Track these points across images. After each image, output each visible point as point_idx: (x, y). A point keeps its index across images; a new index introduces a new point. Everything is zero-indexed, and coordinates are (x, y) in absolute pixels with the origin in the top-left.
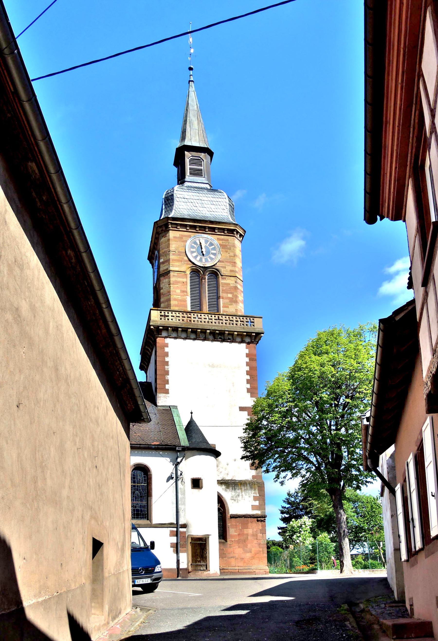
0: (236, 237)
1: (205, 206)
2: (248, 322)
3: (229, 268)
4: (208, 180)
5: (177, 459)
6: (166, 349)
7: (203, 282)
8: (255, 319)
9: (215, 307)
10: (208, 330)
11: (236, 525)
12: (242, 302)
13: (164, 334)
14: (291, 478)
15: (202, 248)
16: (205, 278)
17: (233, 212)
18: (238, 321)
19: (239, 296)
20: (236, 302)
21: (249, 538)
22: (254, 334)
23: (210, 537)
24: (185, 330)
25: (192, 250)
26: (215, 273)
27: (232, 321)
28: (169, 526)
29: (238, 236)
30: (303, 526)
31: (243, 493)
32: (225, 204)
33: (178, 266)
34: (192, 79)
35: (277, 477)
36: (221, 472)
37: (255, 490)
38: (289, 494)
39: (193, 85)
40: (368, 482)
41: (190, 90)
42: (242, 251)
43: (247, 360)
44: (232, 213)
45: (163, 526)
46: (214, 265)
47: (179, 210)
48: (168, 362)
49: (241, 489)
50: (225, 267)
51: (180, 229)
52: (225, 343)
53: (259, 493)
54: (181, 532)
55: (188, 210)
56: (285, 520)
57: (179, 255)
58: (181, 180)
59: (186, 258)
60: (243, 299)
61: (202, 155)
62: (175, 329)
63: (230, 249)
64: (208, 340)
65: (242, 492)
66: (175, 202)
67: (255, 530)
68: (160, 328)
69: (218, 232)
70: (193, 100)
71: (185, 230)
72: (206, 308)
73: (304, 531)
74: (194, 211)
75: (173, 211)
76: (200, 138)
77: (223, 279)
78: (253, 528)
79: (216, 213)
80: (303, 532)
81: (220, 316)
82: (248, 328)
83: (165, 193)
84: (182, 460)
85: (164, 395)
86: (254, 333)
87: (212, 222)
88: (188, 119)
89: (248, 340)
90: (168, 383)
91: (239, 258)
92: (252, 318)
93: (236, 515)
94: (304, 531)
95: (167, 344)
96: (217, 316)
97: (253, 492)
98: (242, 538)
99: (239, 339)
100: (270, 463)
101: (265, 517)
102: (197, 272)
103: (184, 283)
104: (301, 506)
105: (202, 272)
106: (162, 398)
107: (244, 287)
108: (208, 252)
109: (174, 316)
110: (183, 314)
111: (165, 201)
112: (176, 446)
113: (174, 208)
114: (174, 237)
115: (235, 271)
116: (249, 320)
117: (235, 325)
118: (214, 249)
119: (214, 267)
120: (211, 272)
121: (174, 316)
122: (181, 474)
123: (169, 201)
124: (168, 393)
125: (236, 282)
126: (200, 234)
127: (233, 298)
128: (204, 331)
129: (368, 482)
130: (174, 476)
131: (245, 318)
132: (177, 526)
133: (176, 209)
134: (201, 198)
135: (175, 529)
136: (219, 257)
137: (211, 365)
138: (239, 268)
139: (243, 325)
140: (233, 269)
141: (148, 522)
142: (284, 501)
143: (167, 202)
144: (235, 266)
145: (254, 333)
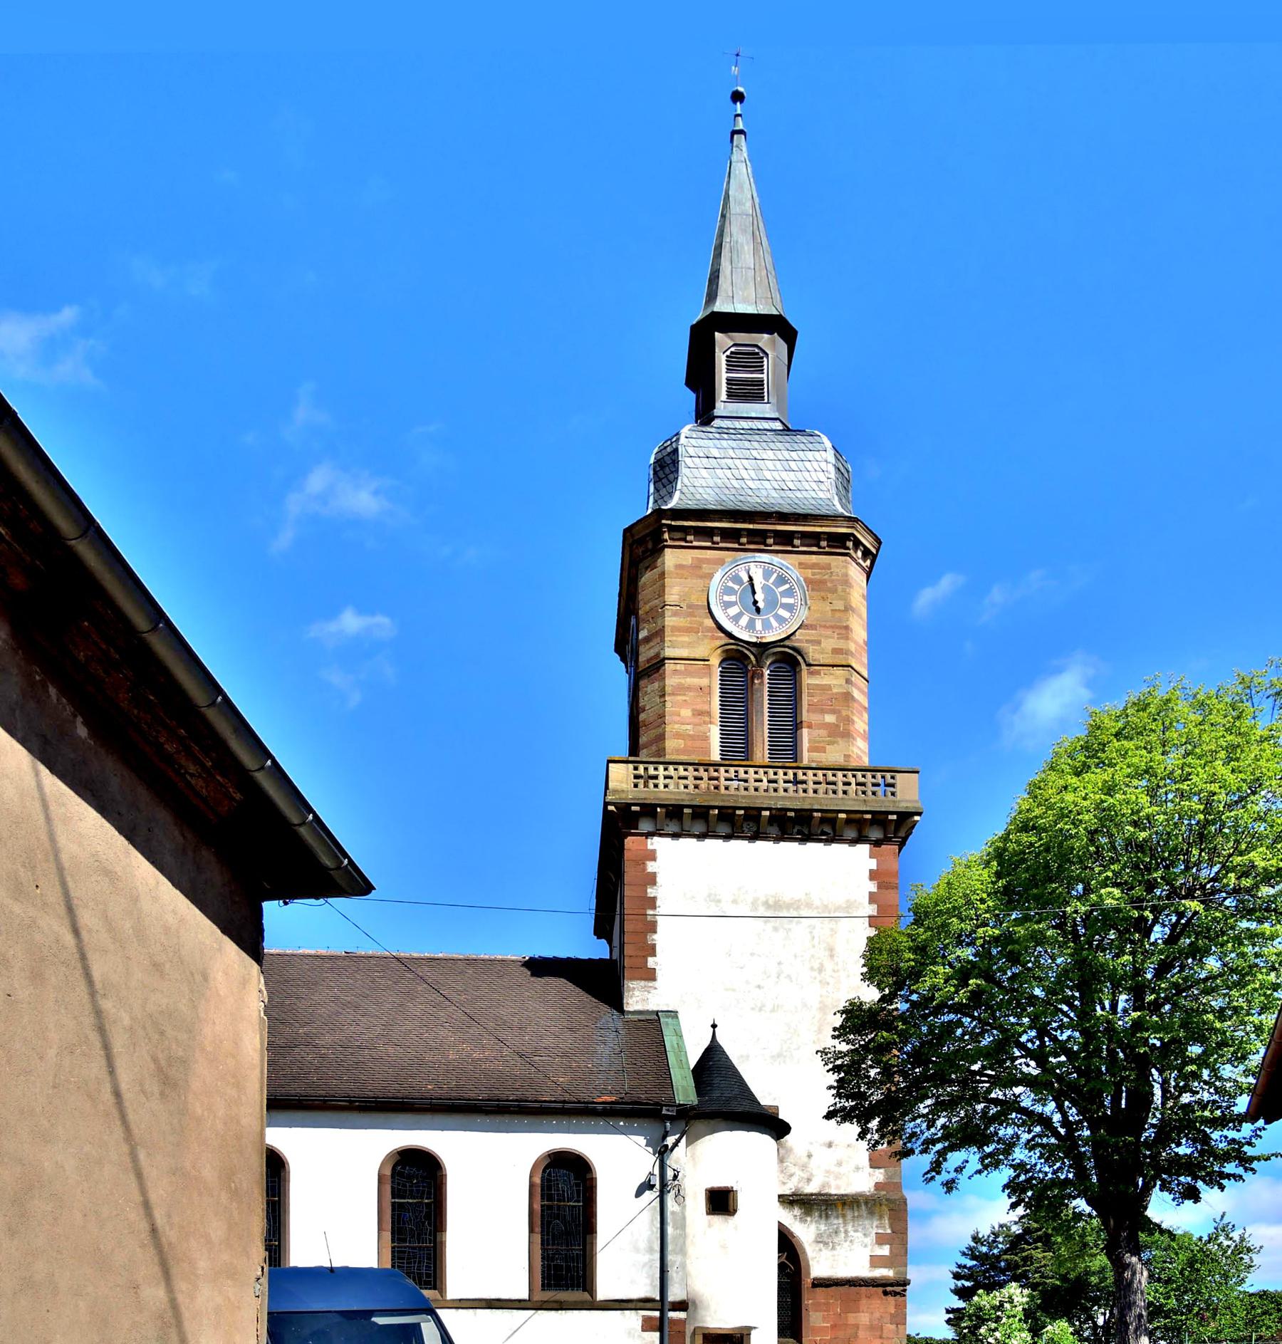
0: (852, 557)
1: (768, 475)
2: (878, 785)
3: (830, 643)
4: (778, 411)
5: (664, 1138)
6: (651, 867)
7: (756, 687)
8: (898, 775)
9: (786, 747)
10: (766, 809)
11: (828, 1304)
12: (863, 738)
13: (645, 826)
14: (979, 1172)
15: (754, 592)
16: (762, 675)
17: (847, 490)
18: (849, 784)
19: (856, 719)
20: (847, 735)
21: (861, 1334)
22: (895, 817)
23: (753, 1332)
24: (701, 813)
25: (726, 598)
26: (788, 660)
27: (834, 783)
28: (641, 1304)
29: (860, 554)
30: (1007, 1306)
31: (850, 1228)
32: (823, 465)
33: (689, 645)
34: (740, 126)
35: (936, 1167)
36: (791, 1175)
37: (881, 1217)
38: (976, 1239)
39: (743, 143)
40: (1228, 1176)
41: (734, 158)
42: (869, 598)
43: (873, 887)
44: (843, 492)
45: (625, 1305)
46: (788, 638)
47: (692, 489)
48: (654, 899)
49: (844, 1216)
50: (819, 643)
51: (695, 544)
52: (811, 845)
53: (891, 1227)
54: (673, 1321)
55: (717, 490)
56: (963, 1293)
57: (691, 615)
58: (705, 415)
59: (709, 622)
60: (867, 728)
61: (764, 340)
62: (675, 811)
63: (834, 591)
64: (766, 838)
65: (845, 1223)
66: (683, 470)
67: (877, 1315)
68: (633, 808)
69: (802, 545)
70: (741, 187)
71: (709, 544)
72: (762, 752)
73: (1009, 1317)
74: (734, 491)
75: (677, 495)
76: (759, 291)
77: (811, 673)
78: (872, 1309)
79: (799, 494)
80: (1004, 1320)
81: (800, 772)
82: (876, 802)
83: (656, 450)
84: (678, 1141)
85: (643, 983)
86: (892, 813)
87: (783, 517)
88: (727, 239)
89: (876, 834)
90: (654, 955)
91: (860, 616)
92: (888, 775)
93: (829, 1279)
94: (1009, 1317)
95: (654, 852)
96: (791, 772)
97: (875, 1223)
98: (841, 1334)
99: (851, 834)
100: (918, 1130)
101: (905, 1283)
102: (739, 660)
103: (704, 691)
104: (1003, 1264)
105: (752, 658)
106: (637, 993)
107: (870, 696)
108: (773, 603)
109: (671, 778)
110: (696, 770)
111: (655, 473)
112: (662, 1106)
113: (679, 487)
114: (679, 566)
115: (847, 652)
116: (880, 781)
117: (840, 794)
118: (789, 593)
119: (787, 643)
120: (778, 657)
121: (671, 778)
122: (675, 1177)
123: (667, 470)
124: (654, 979)
125: (848, 681)
126: (750, 554)
127: (837, 726)
128: (753, 814)
129: (1228, 1176)
130: (657, 1183)
131: (869, 775)
132: (663, 1305)
133: (685, 490)
134: (755, 453)
135: (657, 1314)
136: (802, 615)
137: (771, 902)
138: (856, 643)
139: (864, 793)
140: (841, 644)
141: (586, 1296)
142: (964, 1254)
143: (661, 474)
144: (847, 638)
145: (892, 813)
